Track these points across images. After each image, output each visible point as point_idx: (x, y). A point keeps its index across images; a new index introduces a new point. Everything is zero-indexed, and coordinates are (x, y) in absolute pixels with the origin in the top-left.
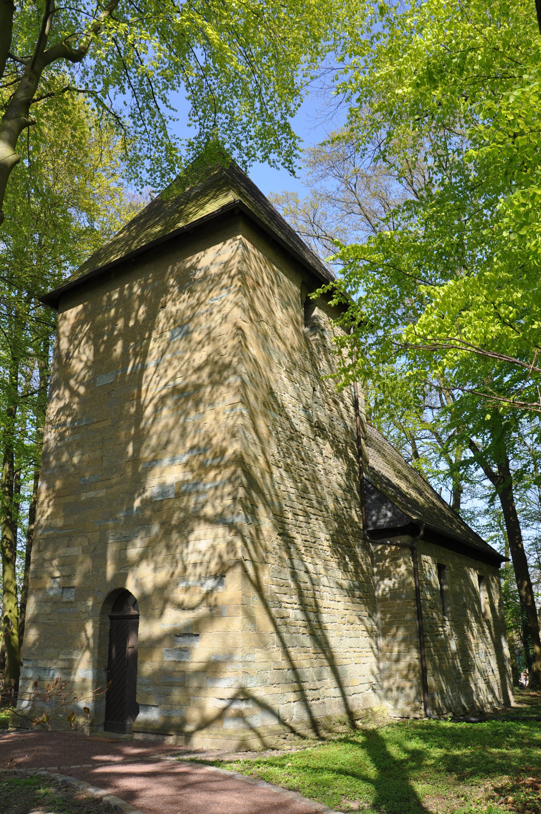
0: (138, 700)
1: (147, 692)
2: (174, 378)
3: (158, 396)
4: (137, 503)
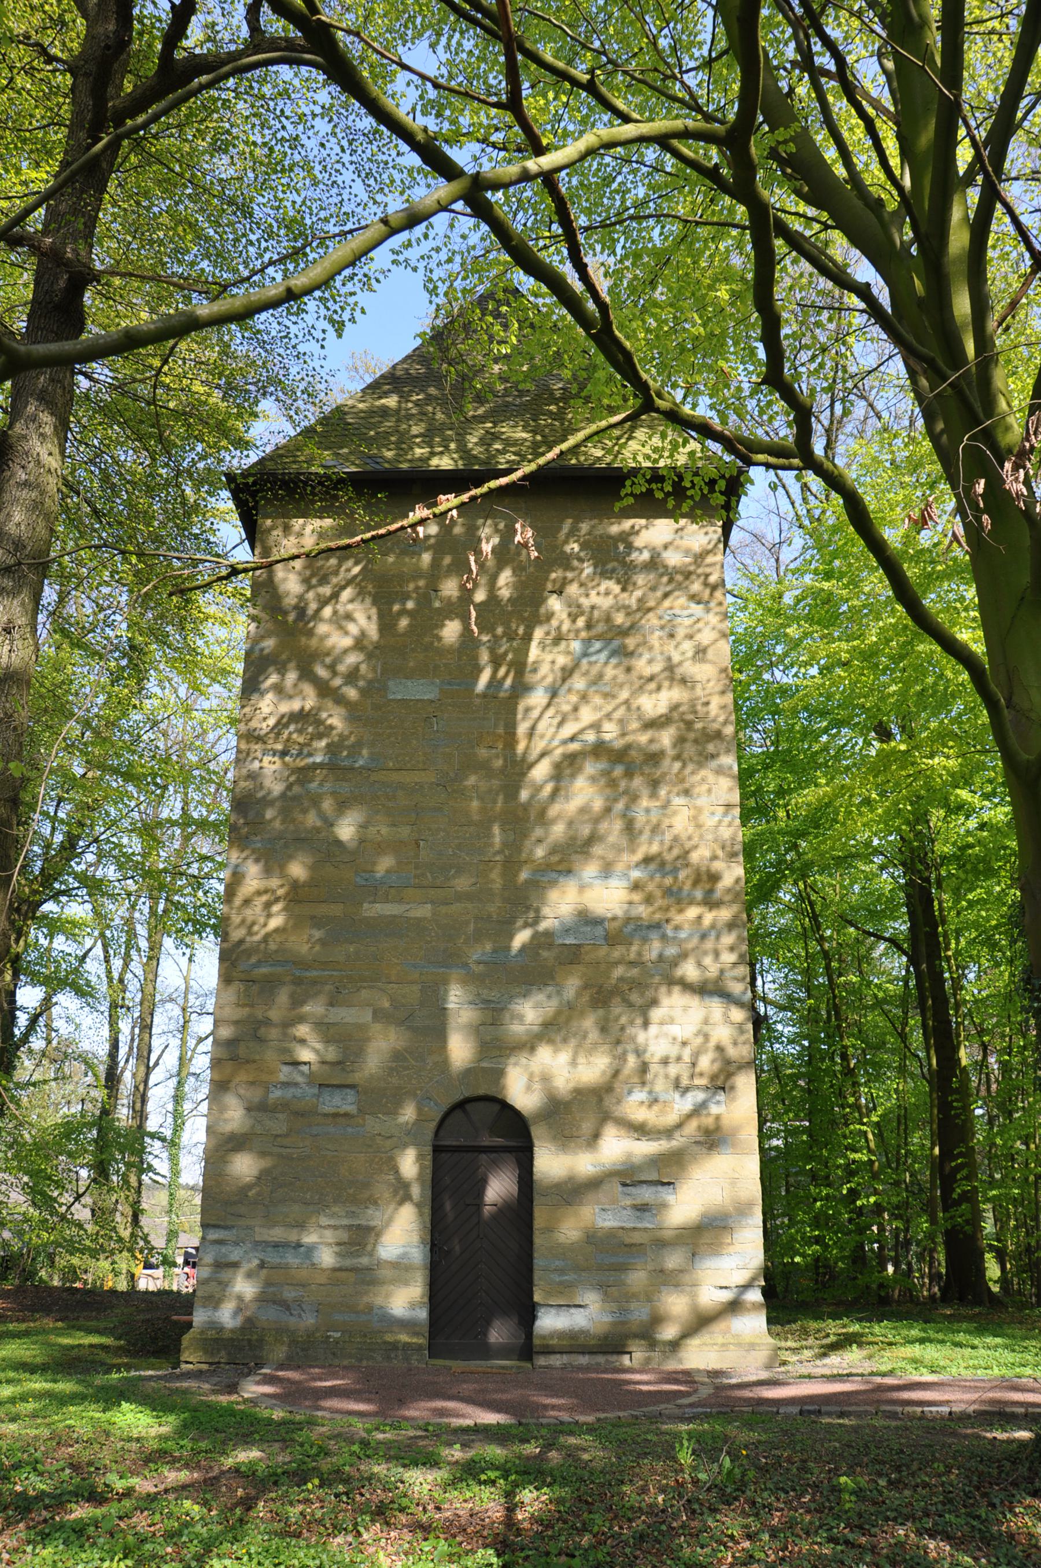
0: (537, 1297)
1: (561, 1283)
2: (596, 726)
3: (559, 752)
4: (522, 938)
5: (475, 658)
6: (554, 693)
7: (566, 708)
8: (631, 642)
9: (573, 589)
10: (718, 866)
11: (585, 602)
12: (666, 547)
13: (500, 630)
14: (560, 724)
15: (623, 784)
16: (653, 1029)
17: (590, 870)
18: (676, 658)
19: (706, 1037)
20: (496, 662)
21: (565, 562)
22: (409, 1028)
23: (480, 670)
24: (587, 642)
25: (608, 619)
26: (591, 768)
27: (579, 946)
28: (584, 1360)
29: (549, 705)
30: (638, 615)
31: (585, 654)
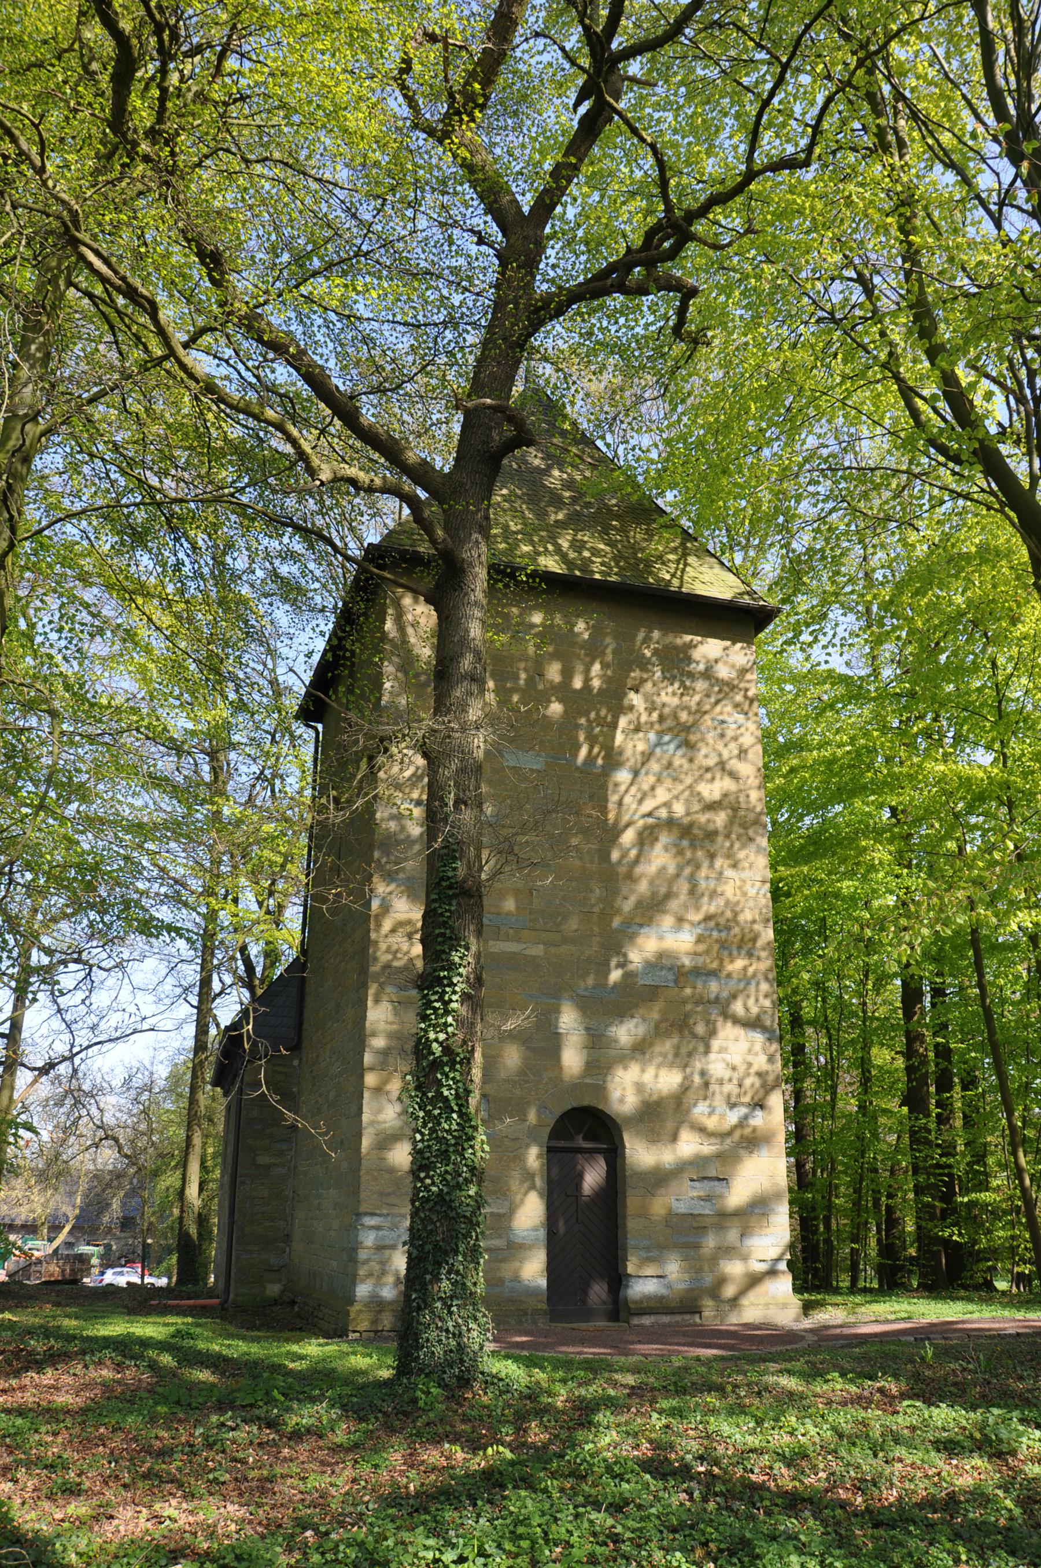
0: (631, 1269)
2: (667, 805)
5: (576, 738)
6: (636, 773)
7: (646, 787)
8: (693, 738)
9: (648, 686)
10: (757, 927)
11: (658, 701)
12: (716, 661)
13: (593, 715)
14: (640, 802)
15: (688, 854)
16: (712, 1056)
17: (668, 921)
18: (726, 755)
19: (750, 1065)
20: (592, 740)
21: (644, 665)
22: (528, 1048)
23: (578, 747)
24: (660, 734)
25: (675, 716)
26: (664, 838)
27: (657, 987)
28: (666, 1319)
29: (631, 784)
30: (697, 716)
31: (658, 744)
